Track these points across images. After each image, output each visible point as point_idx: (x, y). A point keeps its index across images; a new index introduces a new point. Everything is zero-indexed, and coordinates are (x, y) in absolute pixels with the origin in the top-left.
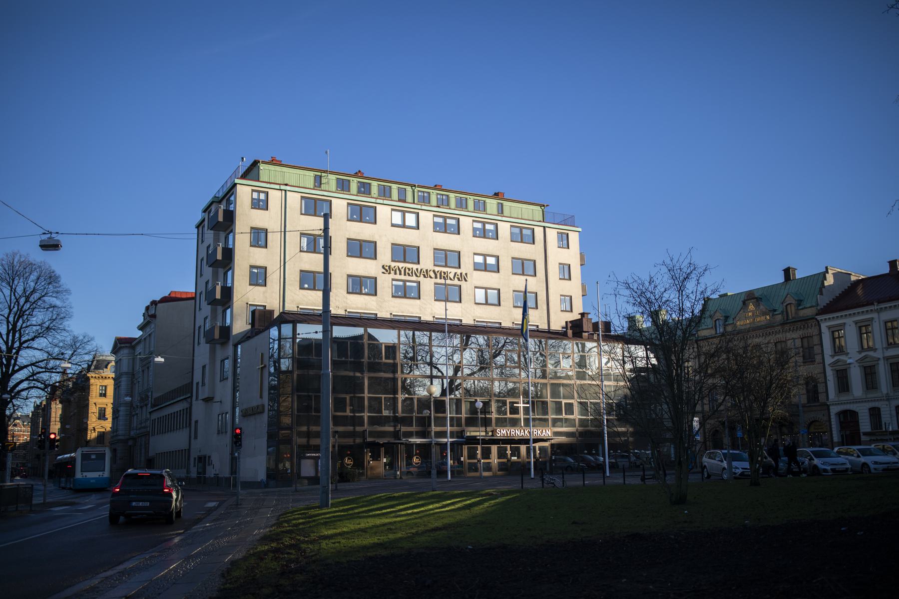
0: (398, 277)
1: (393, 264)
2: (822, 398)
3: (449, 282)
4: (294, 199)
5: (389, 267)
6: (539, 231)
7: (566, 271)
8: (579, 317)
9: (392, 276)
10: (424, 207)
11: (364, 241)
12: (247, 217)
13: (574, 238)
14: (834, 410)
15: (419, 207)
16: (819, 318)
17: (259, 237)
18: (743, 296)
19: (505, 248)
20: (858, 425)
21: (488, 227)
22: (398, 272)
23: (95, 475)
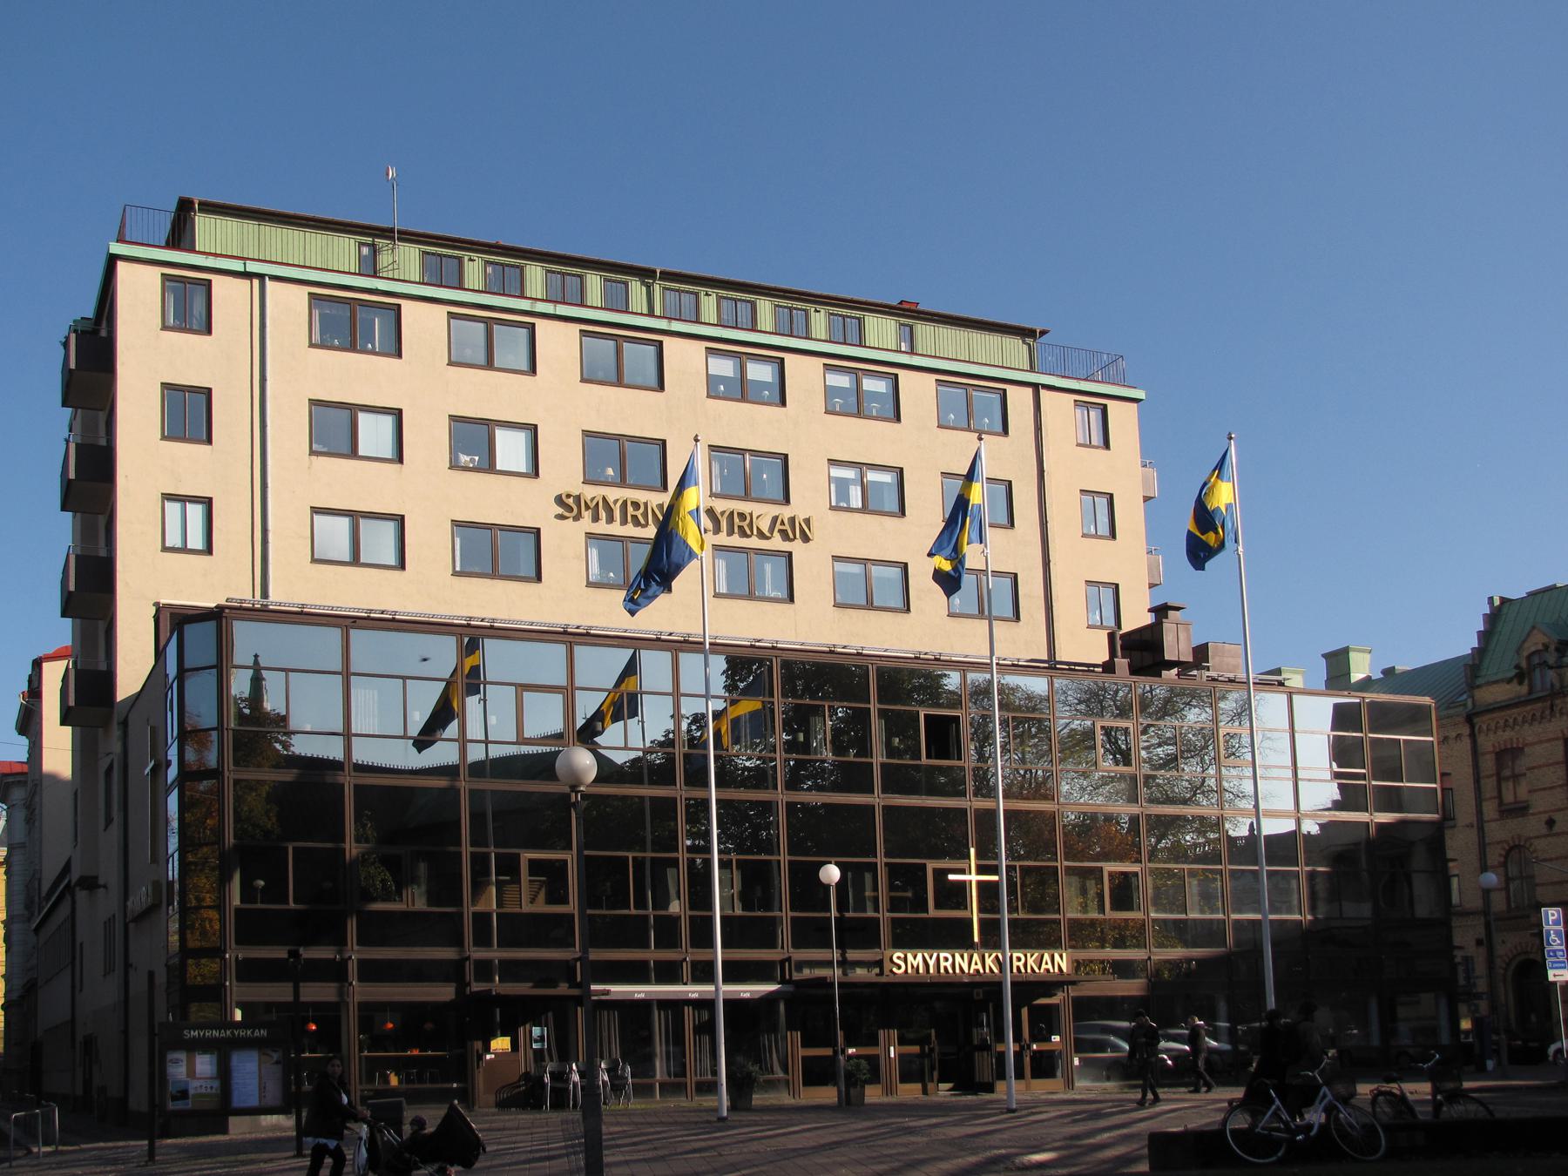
0: (602, 527)
1: (590, 492)
3: (754, 542)
4: (289, 307)
5: (578, 499)
6: (1020, 399)
7: (1103, 513)
9: (586, 524)
10: (677, 326)
11: (632, 439)
12: (147, 357)
13: (1123, 418)
15: (662, 324)
17: (189, 413)
19: (924, 446)
21: (871, 385)
22: (603, 514)
23: (481, 1086)
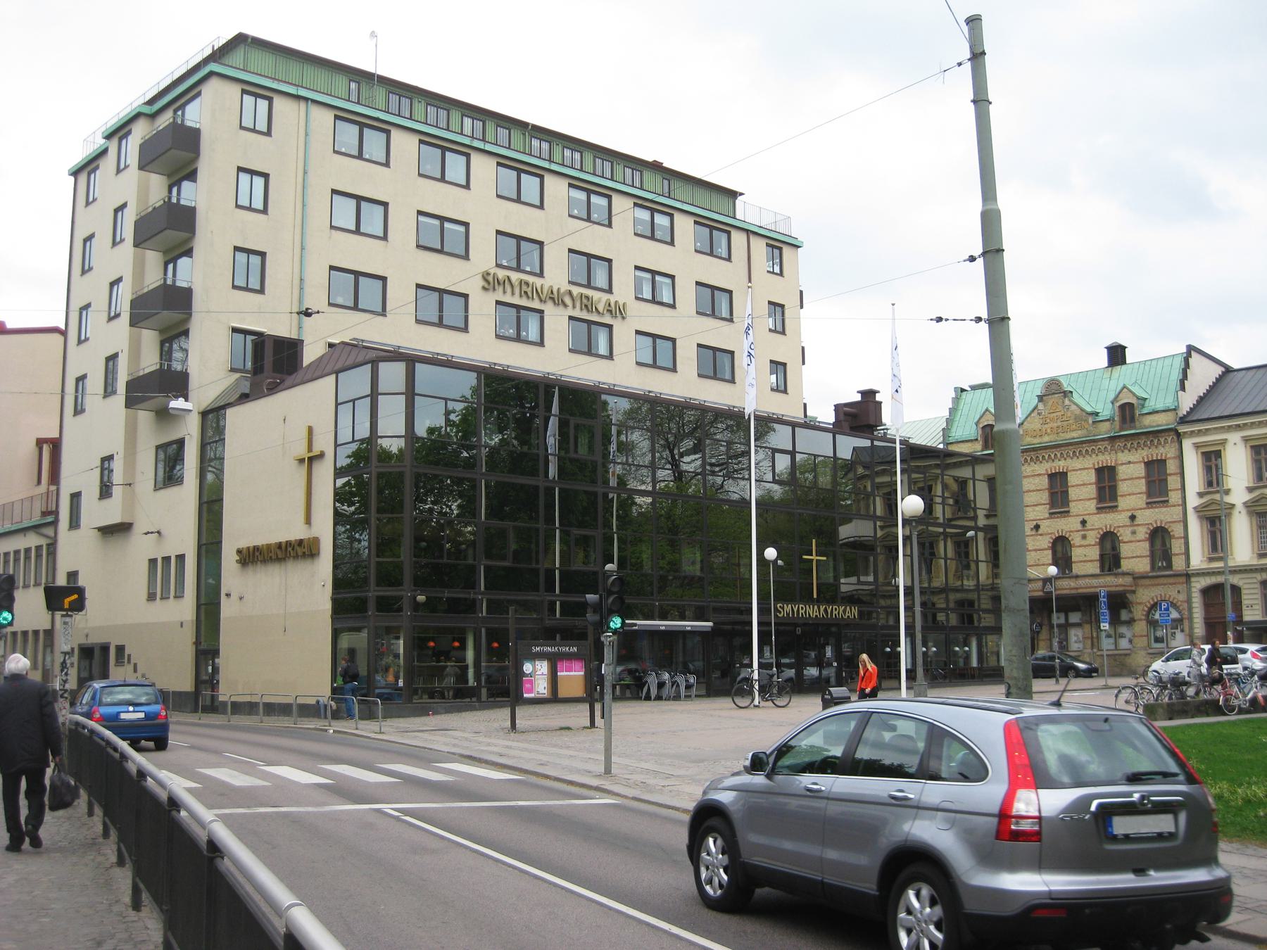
2: (1178, 564)
8: (858, 398)
14: (1199, 584)
16: (1182, 429)
18: (1040, 384)
20: (180, 693)
